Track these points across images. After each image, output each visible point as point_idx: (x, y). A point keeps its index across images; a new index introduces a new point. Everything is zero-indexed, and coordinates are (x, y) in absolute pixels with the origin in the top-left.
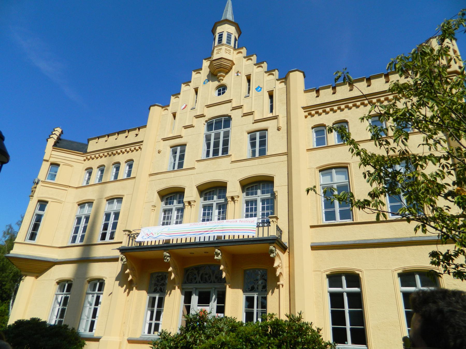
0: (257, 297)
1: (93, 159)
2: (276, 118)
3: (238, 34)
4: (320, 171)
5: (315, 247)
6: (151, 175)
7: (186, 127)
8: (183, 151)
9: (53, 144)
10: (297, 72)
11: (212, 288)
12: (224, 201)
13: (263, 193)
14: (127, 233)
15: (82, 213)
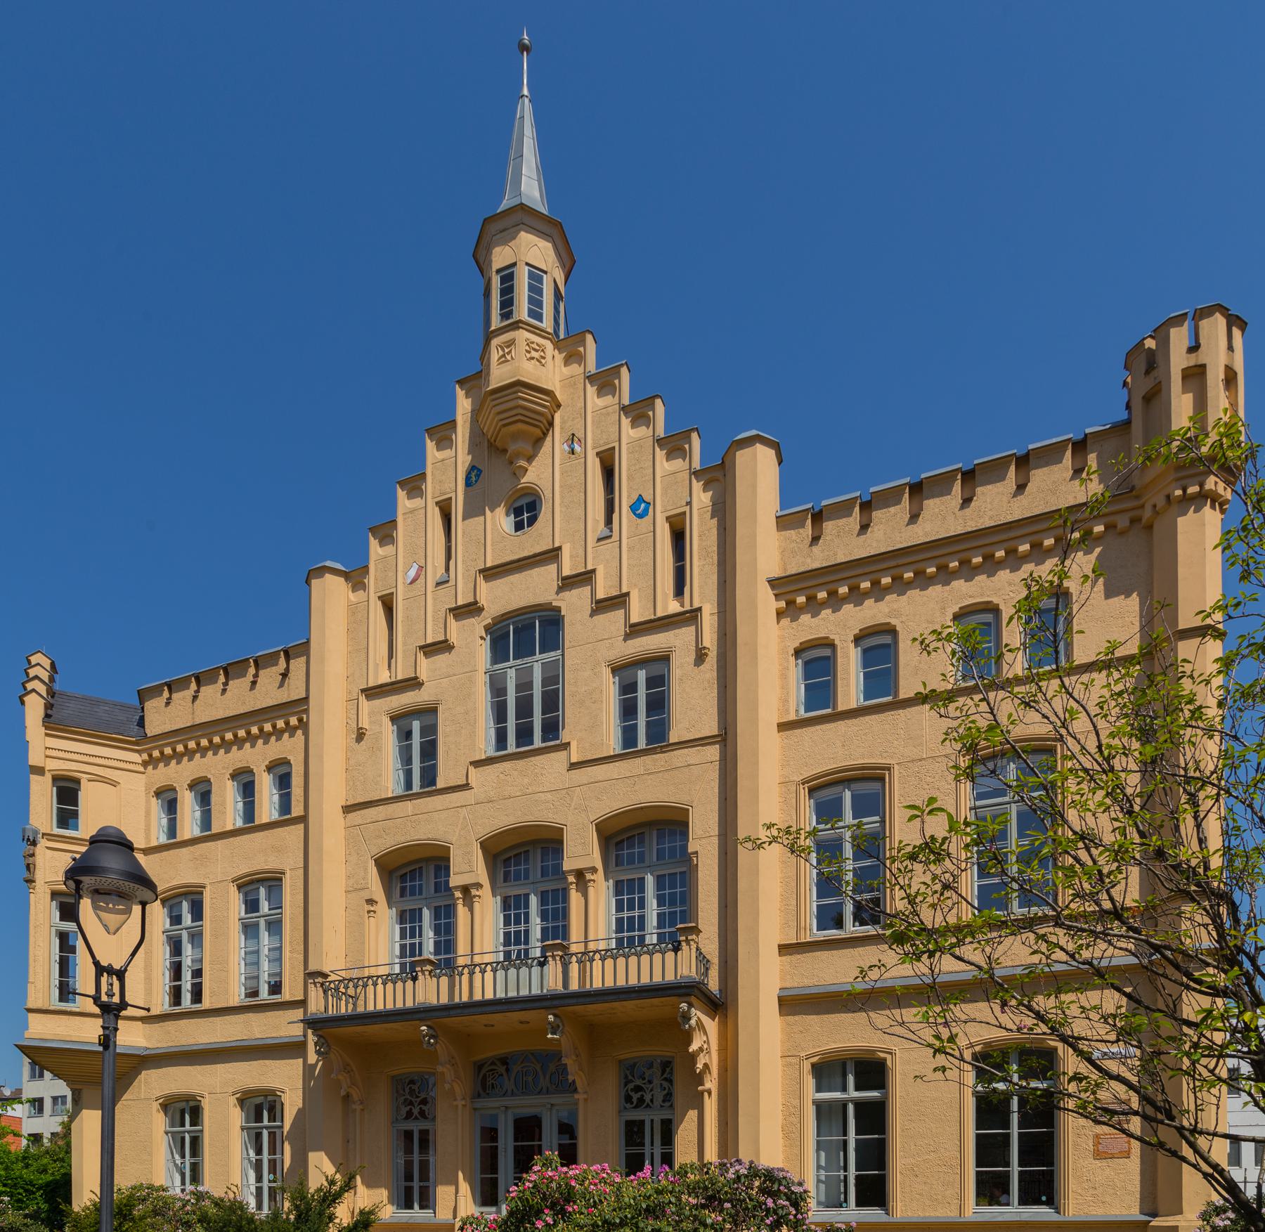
2: (691, 617)
3: (563, 265)
8: (430, 731)
9: (41, 712)
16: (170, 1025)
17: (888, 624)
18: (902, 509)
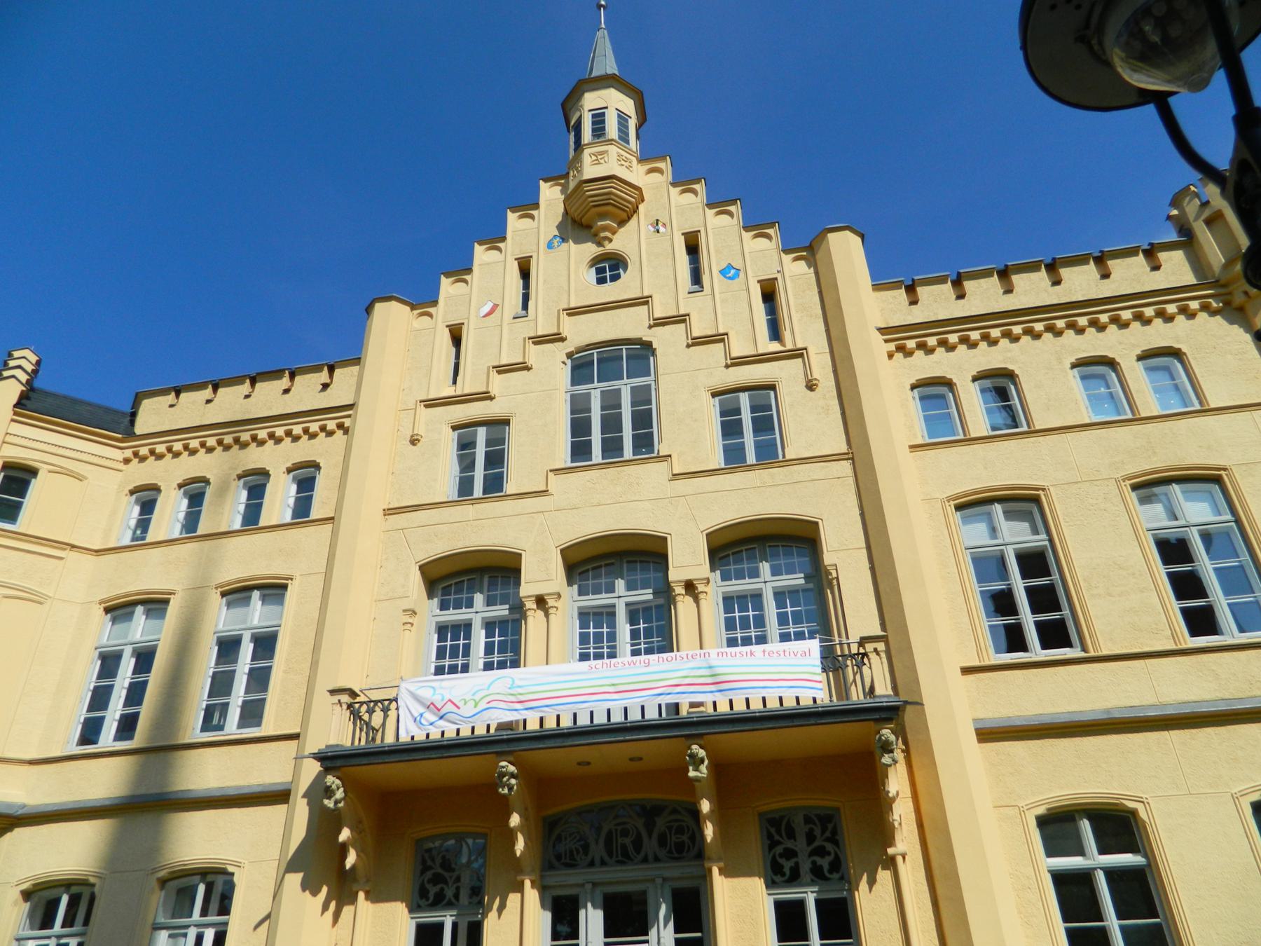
0: (455, 925)
1: (160, 457)
4: (959, 508)
5: (987, 734)
6: (389, 512)
7: (503, 369)
10: (847, 232)
11: (653, 880)
12: (651, 597)
13: (490, 602)
14: (345, 698)
15: (126, 636)
17: (1005, 369)
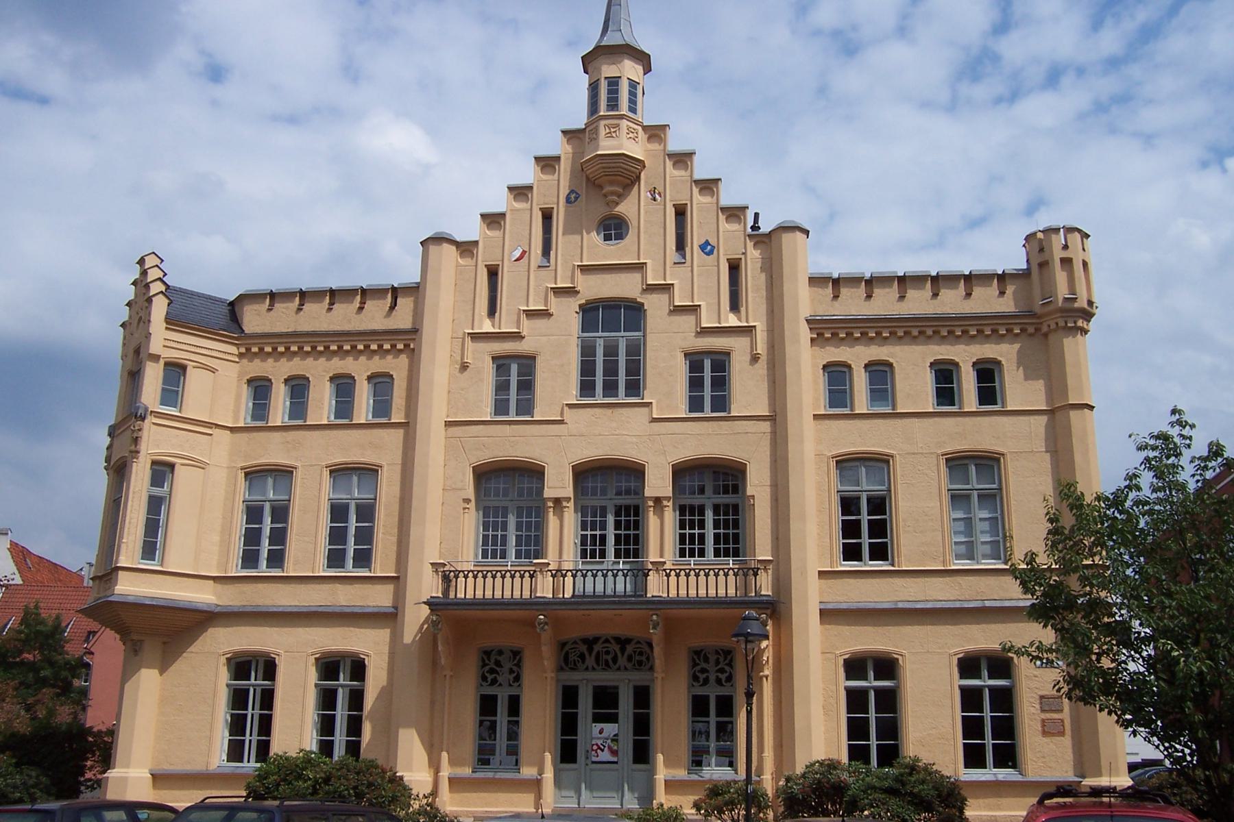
16: (248, 588)
18: (894, 290)
